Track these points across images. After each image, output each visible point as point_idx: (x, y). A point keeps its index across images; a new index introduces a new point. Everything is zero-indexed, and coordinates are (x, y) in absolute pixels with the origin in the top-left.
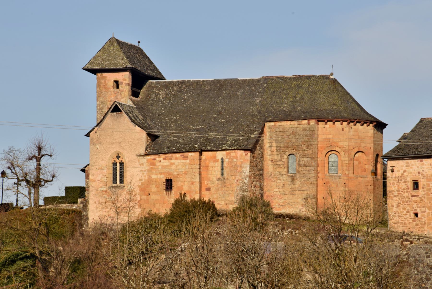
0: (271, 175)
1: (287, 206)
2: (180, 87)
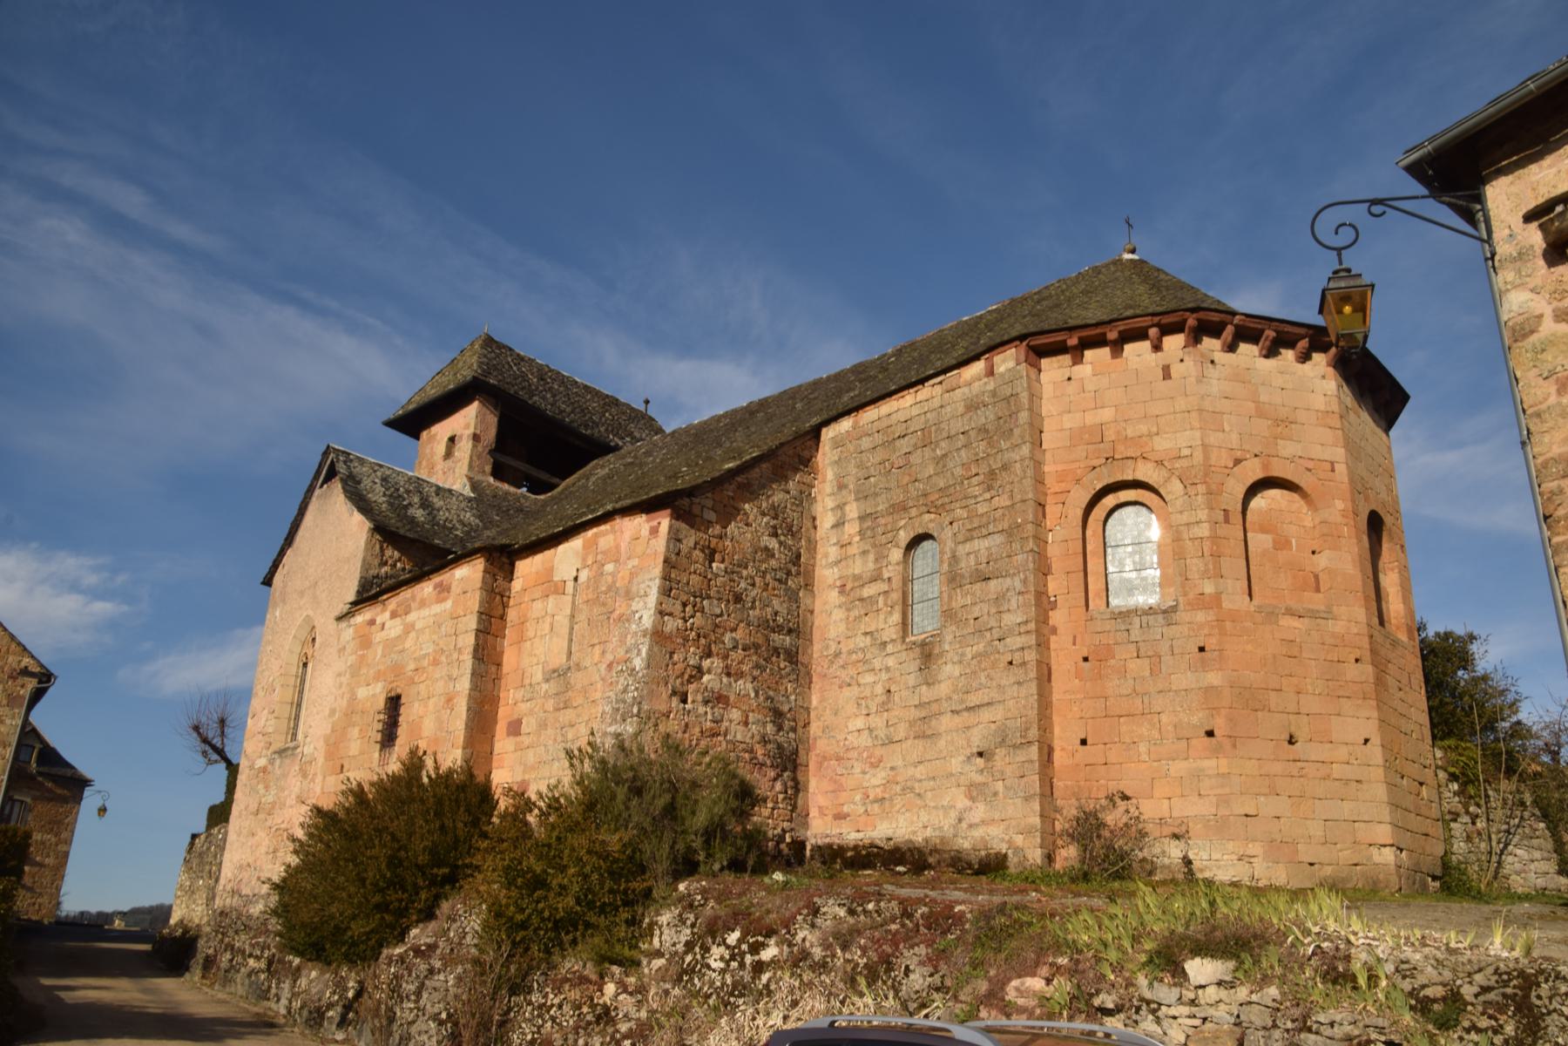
0: (837, 655)
1: (898, 801)
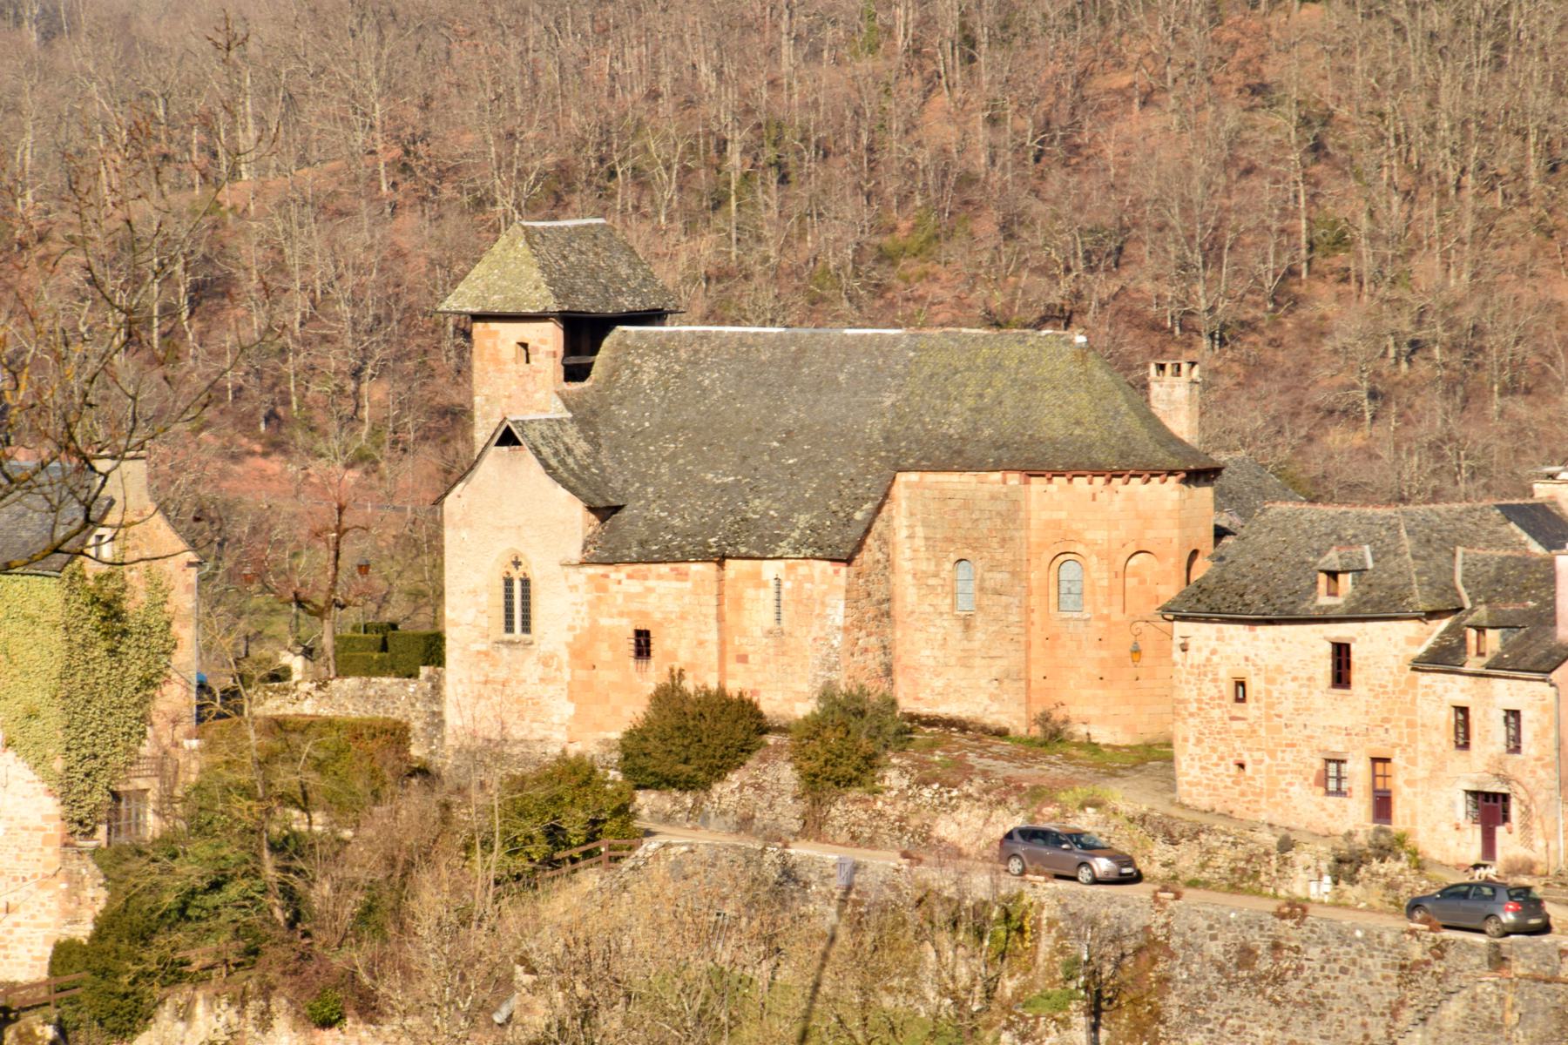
2: (696, 352)
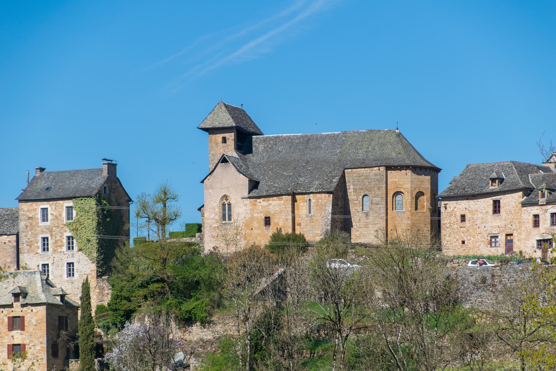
1: (362, 237)
